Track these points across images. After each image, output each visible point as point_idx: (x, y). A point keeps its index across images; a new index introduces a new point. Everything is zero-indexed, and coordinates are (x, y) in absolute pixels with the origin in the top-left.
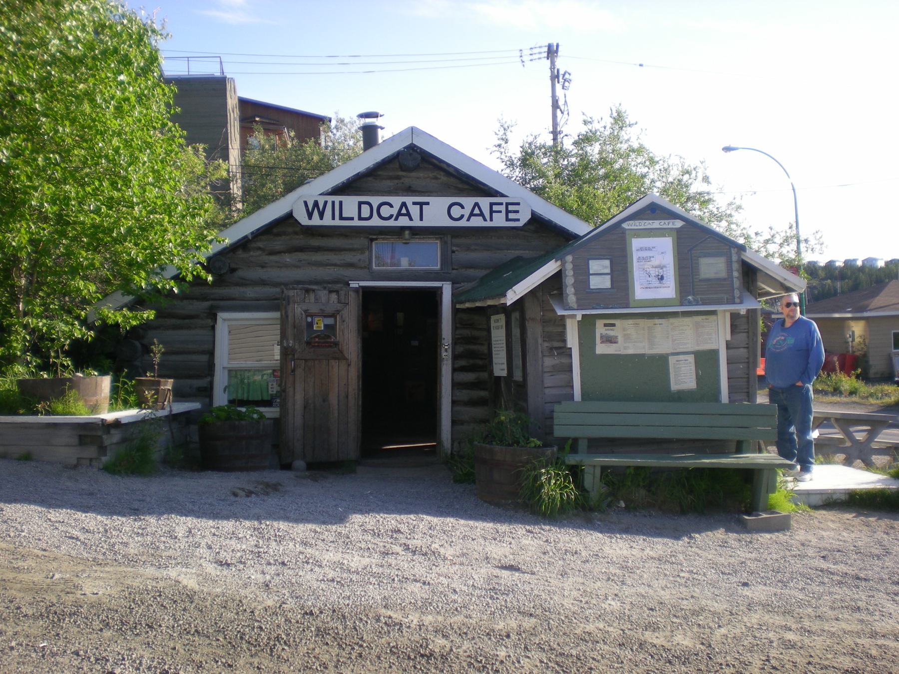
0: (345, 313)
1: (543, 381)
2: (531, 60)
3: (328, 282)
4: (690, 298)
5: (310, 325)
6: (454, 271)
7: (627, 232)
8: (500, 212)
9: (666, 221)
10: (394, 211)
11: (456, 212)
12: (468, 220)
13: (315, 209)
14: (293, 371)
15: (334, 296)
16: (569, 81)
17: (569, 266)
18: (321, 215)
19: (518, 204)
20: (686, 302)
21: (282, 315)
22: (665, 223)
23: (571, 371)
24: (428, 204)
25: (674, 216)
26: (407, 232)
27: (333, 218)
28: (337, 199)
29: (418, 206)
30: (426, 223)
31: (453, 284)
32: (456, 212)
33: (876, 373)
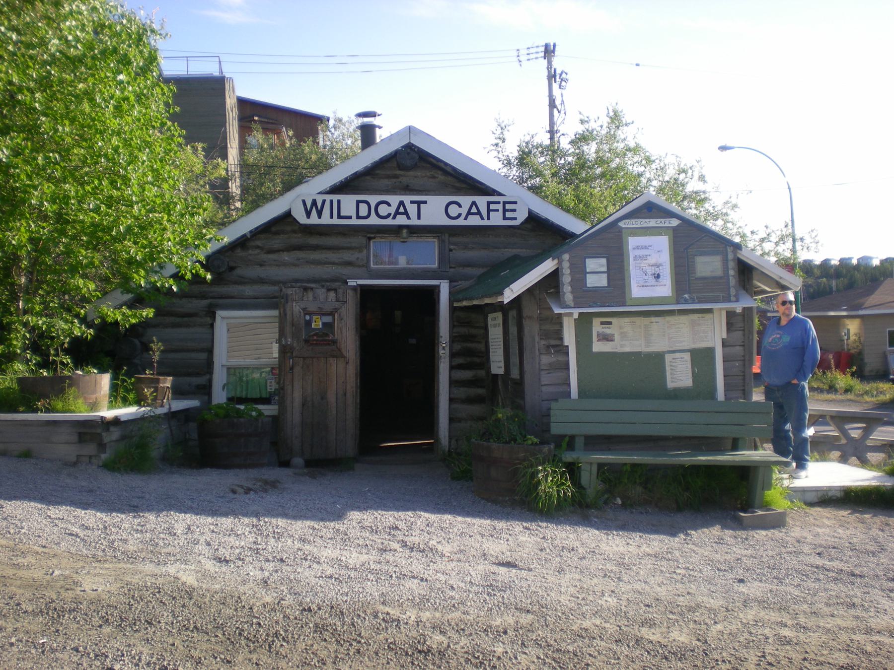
0: (343, 311)
1: (540, 379)
2: (528, 60)
3: (327, 281)
4: (686, 296)
5: (309, 323)
7: (624, 231)
8: (497, 210)
9: (663, 220)
10: (392, 210)
11: (454, 210)
12: (466, 219)
13: (313, 207)
14: (292, 369)
16: (566, 81)
17: (566, 265)
18: (320, 214)
19: (515, 203)
20: (682, 300)
21: (280, 313)
22: (661, 222)
24: (425, 202)
25: (670, 214)
26: (405, 231)
27: (332, 217)
28: (335, 198)
29: (416, 205)
30: (423, 222)
31: (450, 282)
32: (454, 210)
33: (871, 371)
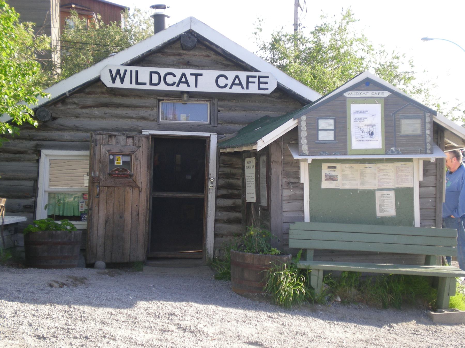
0: (138, 153)
4: (393, 149)
5: (112, 161)
6: (219, 125)
8: (254, 83)
9: (377, 92)
10: (177, 80)
11: (222, 81)
12: (231, 88)
14: (98, 195)
15: (130, 141)
17: (304, 124)
23: (303, 200)
24: (201, 75)
26: (185, 96)
27: (131, 83)
28: (134, 68)
29: (194, 77)
30: (200, 89)
31: (218, 134)
32: (222, 81)
